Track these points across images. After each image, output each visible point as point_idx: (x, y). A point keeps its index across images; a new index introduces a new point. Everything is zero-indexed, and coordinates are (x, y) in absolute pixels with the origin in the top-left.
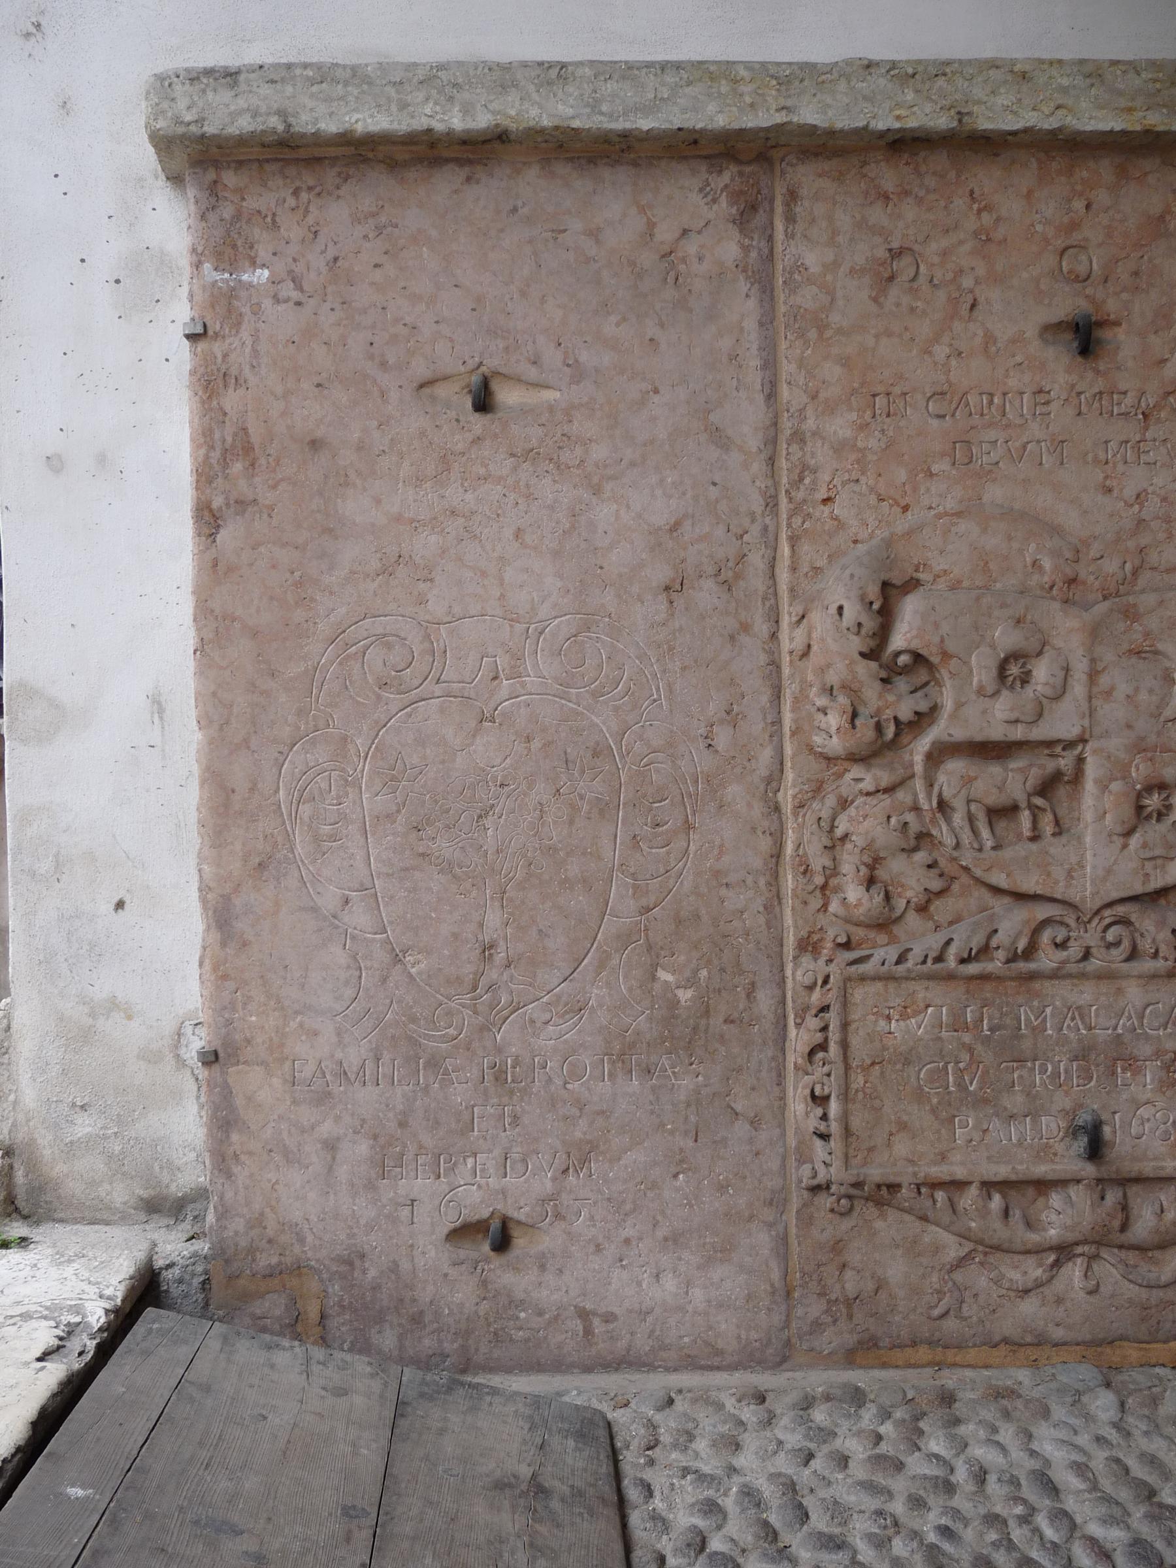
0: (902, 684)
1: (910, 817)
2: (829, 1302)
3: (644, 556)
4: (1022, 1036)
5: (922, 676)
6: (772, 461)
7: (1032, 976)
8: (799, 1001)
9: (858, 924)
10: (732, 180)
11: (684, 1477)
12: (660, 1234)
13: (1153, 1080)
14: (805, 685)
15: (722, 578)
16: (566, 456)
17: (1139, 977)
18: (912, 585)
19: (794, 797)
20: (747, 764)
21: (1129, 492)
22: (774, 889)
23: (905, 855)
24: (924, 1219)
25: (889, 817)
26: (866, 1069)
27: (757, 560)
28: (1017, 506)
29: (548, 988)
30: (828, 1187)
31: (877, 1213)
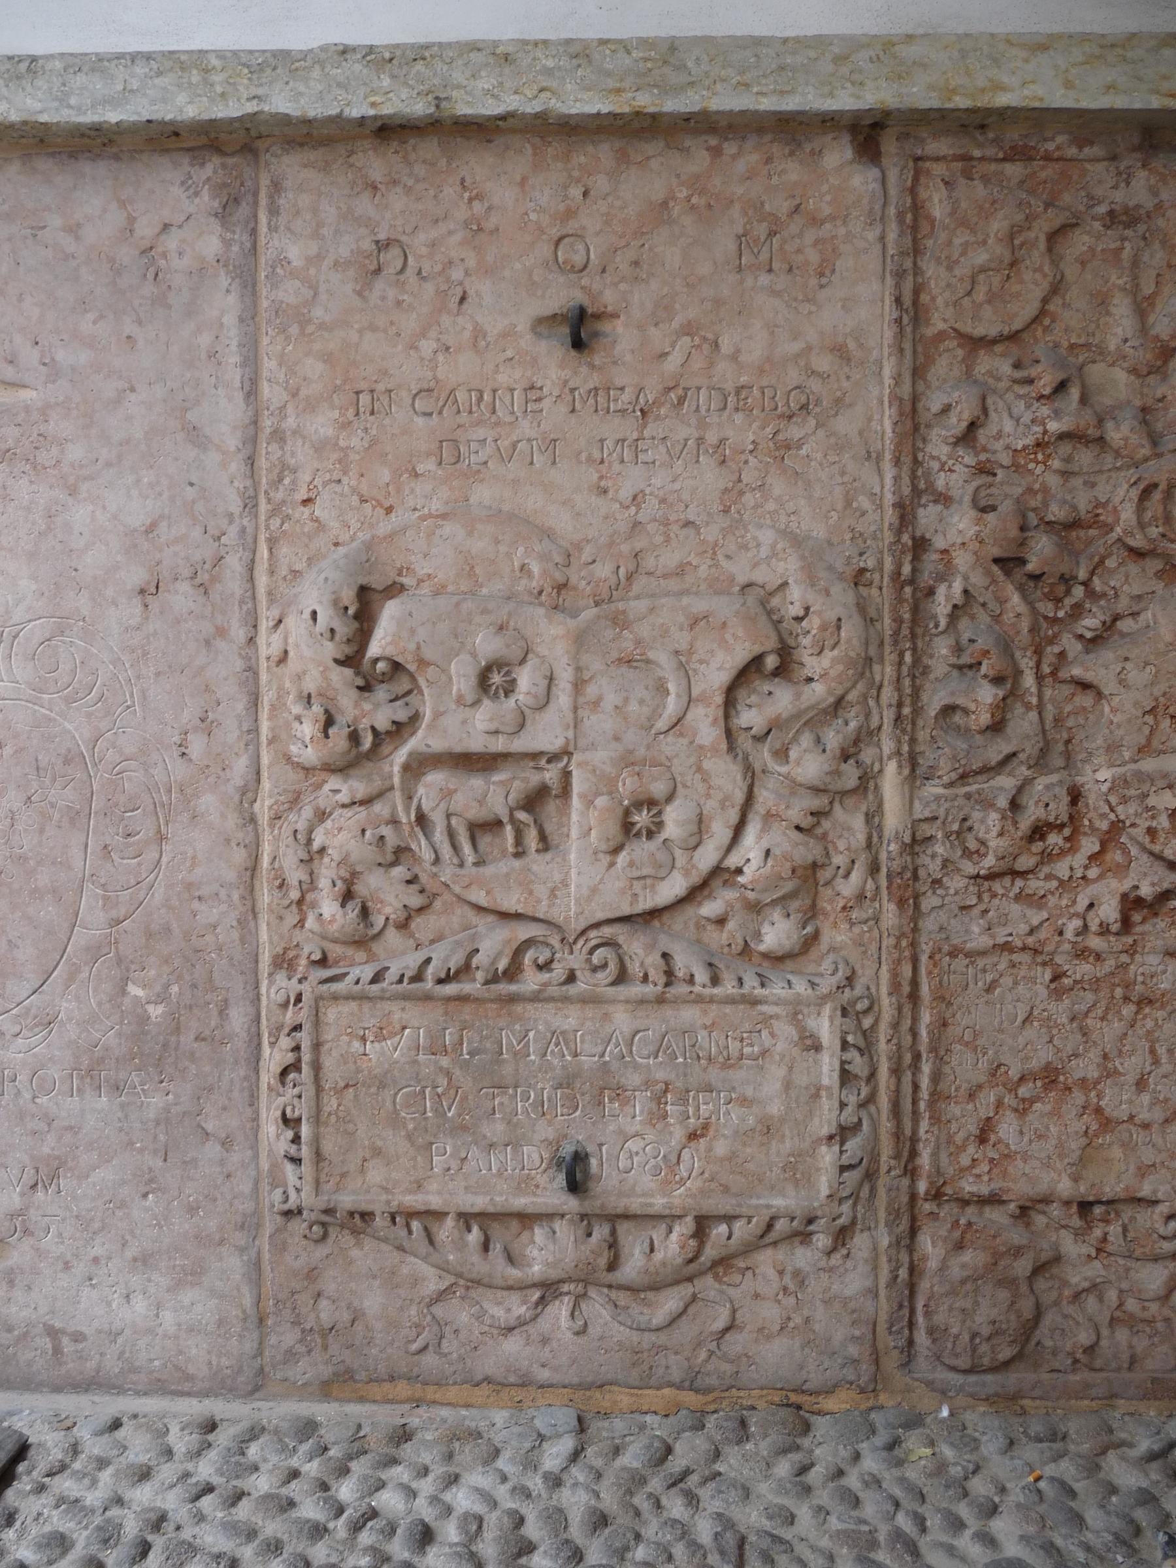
0: (381, 693)
1: (386, 831)
2: (303, 1331)
3: (119, 558)
4: (504, 1061)
5: (404, 685)
6: (251, 461)
7: (513, 999)
8: (273, 1020)
9: (335, 941)
10: (215, 172)
11: (57, 1506)
12: (129, 1254)
13: (642, 1112)
14: (282, 693)
15: (198, 581)
16: (43, 457)
17: (627, 1002)
18: (394, 590)
19: (270, 808)
20: (221, 774)
21: (625, 494)
22: (249, 903)
23: (382, 870)
24: (400, 1248)
25: (363, 831)
26: (340, 1091)
27: (234, 563)
28: (506, 507)
29: (18, 1000)
30: (300, 1212)
31: (352, 1241)
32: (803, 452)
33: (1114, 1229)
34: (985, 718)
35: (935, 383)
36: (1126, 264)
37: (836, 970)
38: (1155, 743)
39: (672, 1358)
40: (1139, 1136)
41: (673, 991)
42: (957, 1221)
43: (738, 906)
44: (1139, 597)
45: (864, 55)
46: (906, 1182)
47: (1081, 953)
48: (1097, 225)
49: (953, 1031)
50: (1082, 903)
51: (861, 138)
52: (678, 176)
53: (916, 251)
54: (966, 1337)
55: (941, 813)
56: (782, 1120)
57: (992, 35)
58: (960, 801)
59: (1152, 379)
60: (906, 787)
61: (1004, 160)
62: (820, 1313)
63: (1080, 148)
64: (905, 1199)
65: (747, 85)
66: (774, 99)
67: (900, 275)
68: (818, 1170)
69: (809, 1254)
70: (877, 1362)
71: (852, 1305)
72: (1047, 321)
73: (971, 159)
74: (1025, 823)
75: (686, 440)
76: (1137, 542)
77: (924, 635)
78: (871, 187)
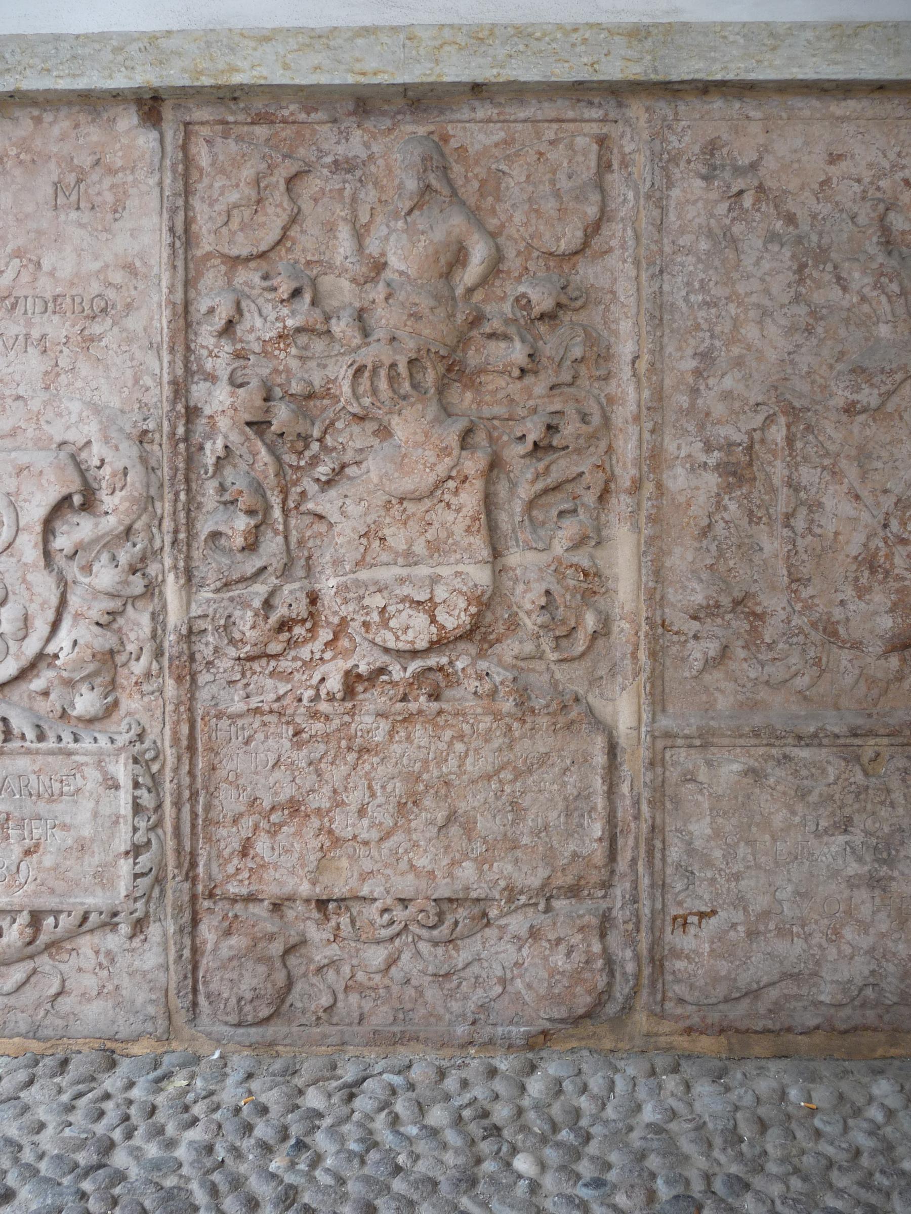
32: (103, 344)
33: (344, 920)
34: (239, 541)
35: (204, 291)
36: (347, 201)
37: (130, 729)
38: (368, 559)
39: (20, 1015)
40: (363, 851)
41: (10, 746)
42: (227, 914)
43: (56, 682)
44: (361, 450)
45: (133, 48)
46: (187, 885)
47: (315, 715)
48: (325, 171)
49: (221, 773)
50: (317, 677)
51: (146, 108)
52: (10, 139)
53: (188, 192)
54: (234, 1000)
55: (211, 612)
56: (92, 841)
57: (230, 30)
58: (225, 603)
59: (368, 286)
60: (183, 593)
61: (252, 123)
62: (126, 982)
63: (308, 114)
64: (186, 898)
65: (48, 70)
66: (68, 80)
67: (174, 211)
68: (119, 877)
69: (117, 939)
70: (170, 1018)
71: (149, 976)
72: (289, 244)
73: (227, 123)
74: (274, 618)
75: (17, 336)
76: (355, 409)
77: (197, 480)
78: (151, 145)
